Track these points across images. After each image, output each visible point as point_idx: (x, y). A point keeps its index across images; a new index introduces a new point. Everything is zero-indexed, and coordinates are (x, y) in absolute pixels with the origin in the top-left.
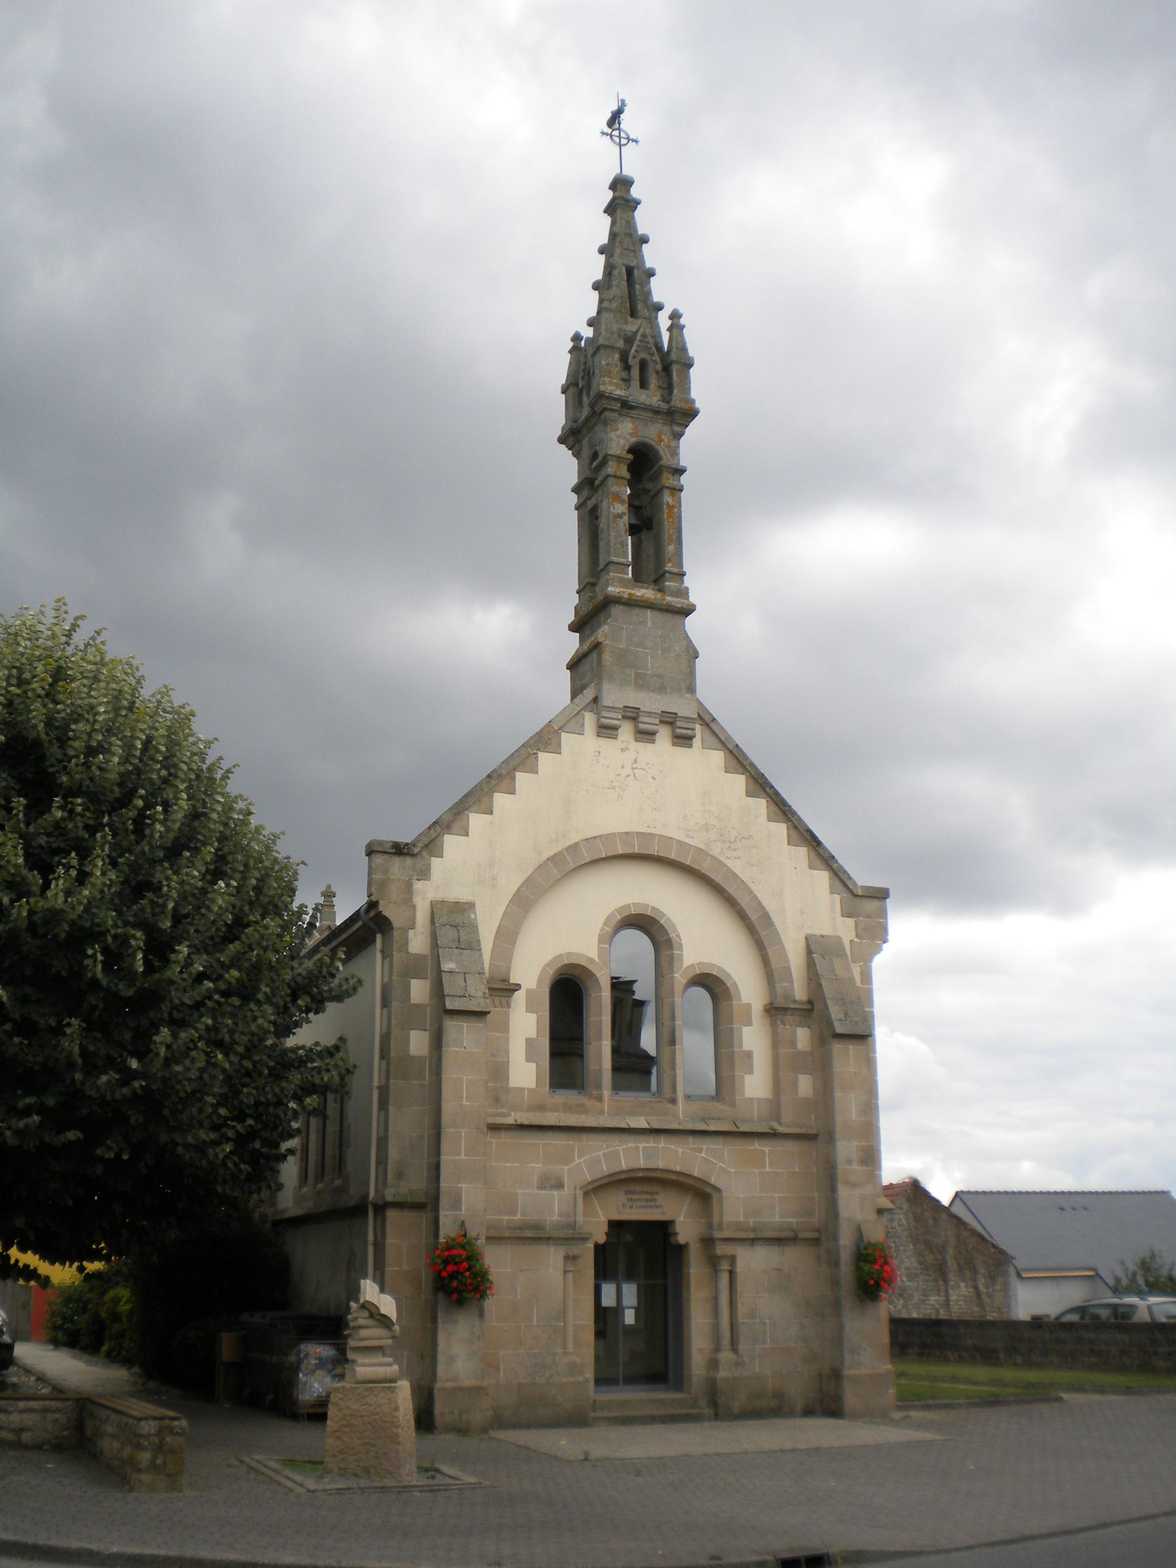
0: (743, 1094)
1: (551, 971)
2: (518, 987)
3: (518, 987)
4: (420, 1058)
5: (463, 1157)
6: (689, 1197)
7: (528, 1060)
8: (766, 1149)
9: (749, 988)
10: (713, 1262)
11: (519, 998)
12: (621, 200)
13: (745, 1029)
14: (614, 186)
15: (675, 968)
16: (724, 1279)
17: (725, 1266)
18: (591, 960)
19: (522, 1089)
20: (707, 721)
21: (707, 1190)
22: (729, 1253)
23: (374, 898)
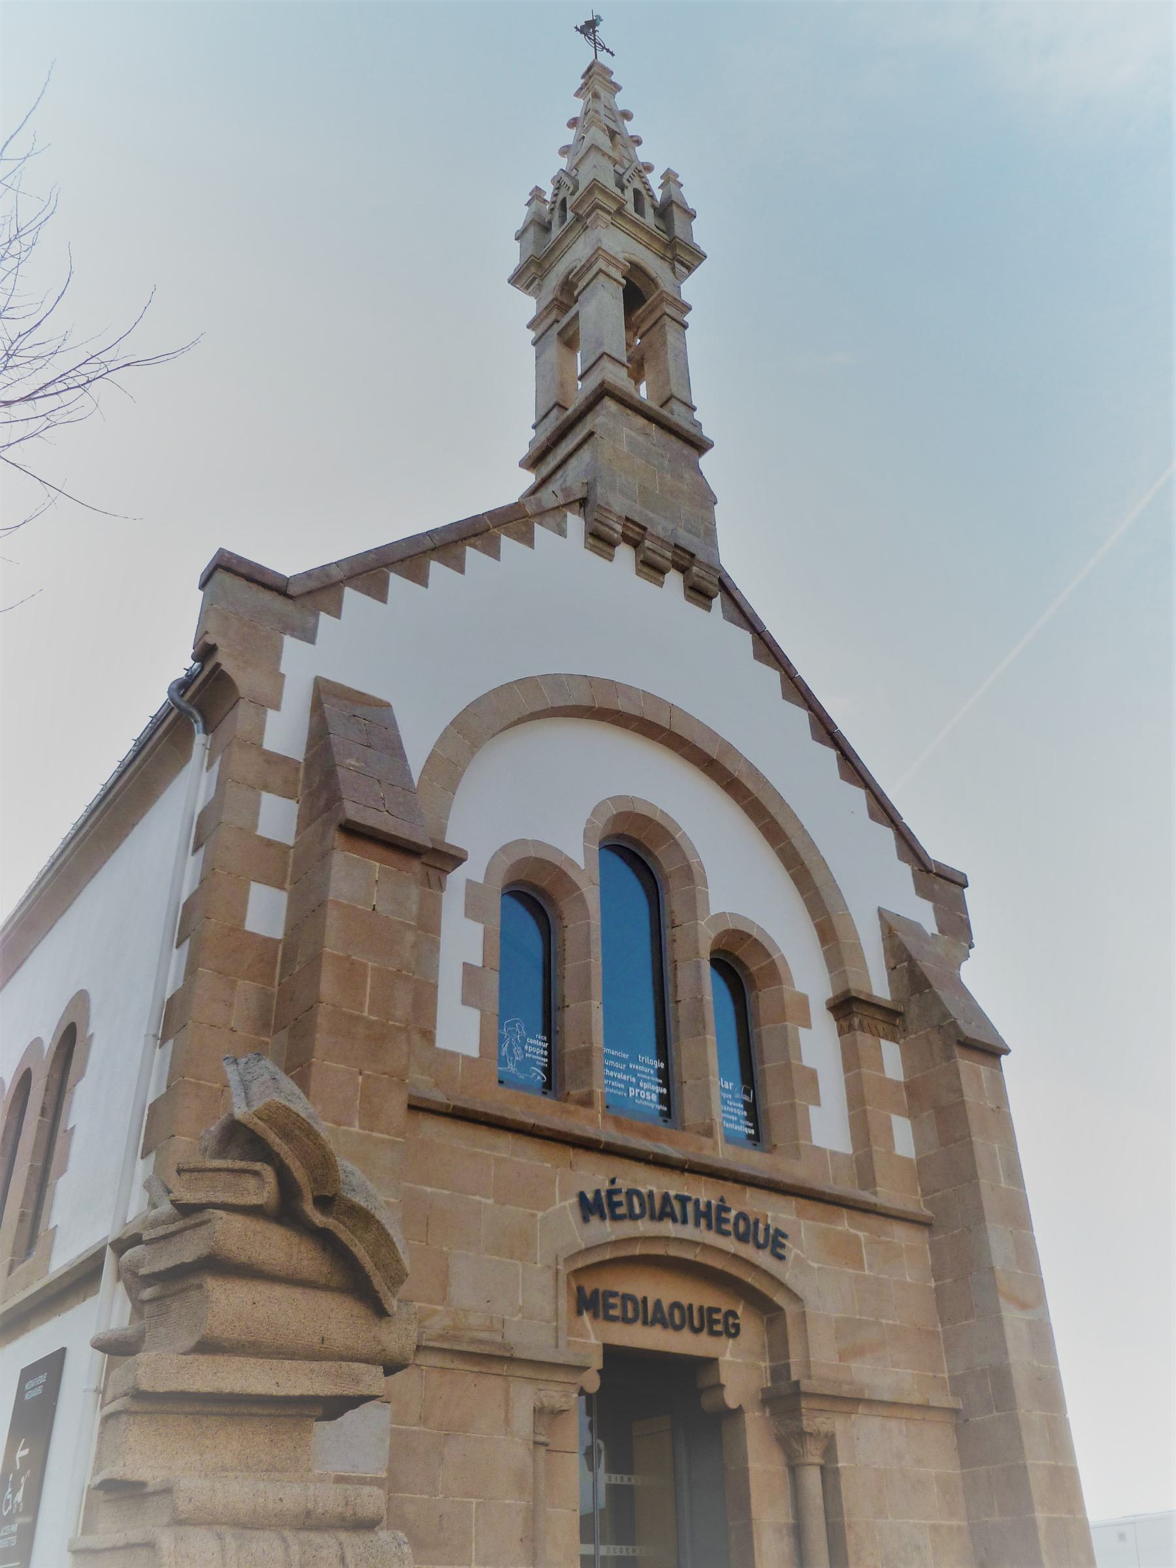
0: (810, 1138)
1: (507, 862)
2: (455, 859)
3: (455, 859)
4: (267, 940)
5: (370, 964)
6: (742, 1303)
7: (465, 1002)
8: (862, 1235)
9: (808, 976)
10: (790, 1442)
11: (457, 879)
12: (597, 81)
13: (803, 1032)
14: (546, 258)
15: (699, 912)
16: (812, 1479)
17: (813, 1454)
18: (573, 864)
19: (454, 1055)
20: (726, 588)
21: (779, 1299)
22: (825, 1428)
23: (210, 640)
